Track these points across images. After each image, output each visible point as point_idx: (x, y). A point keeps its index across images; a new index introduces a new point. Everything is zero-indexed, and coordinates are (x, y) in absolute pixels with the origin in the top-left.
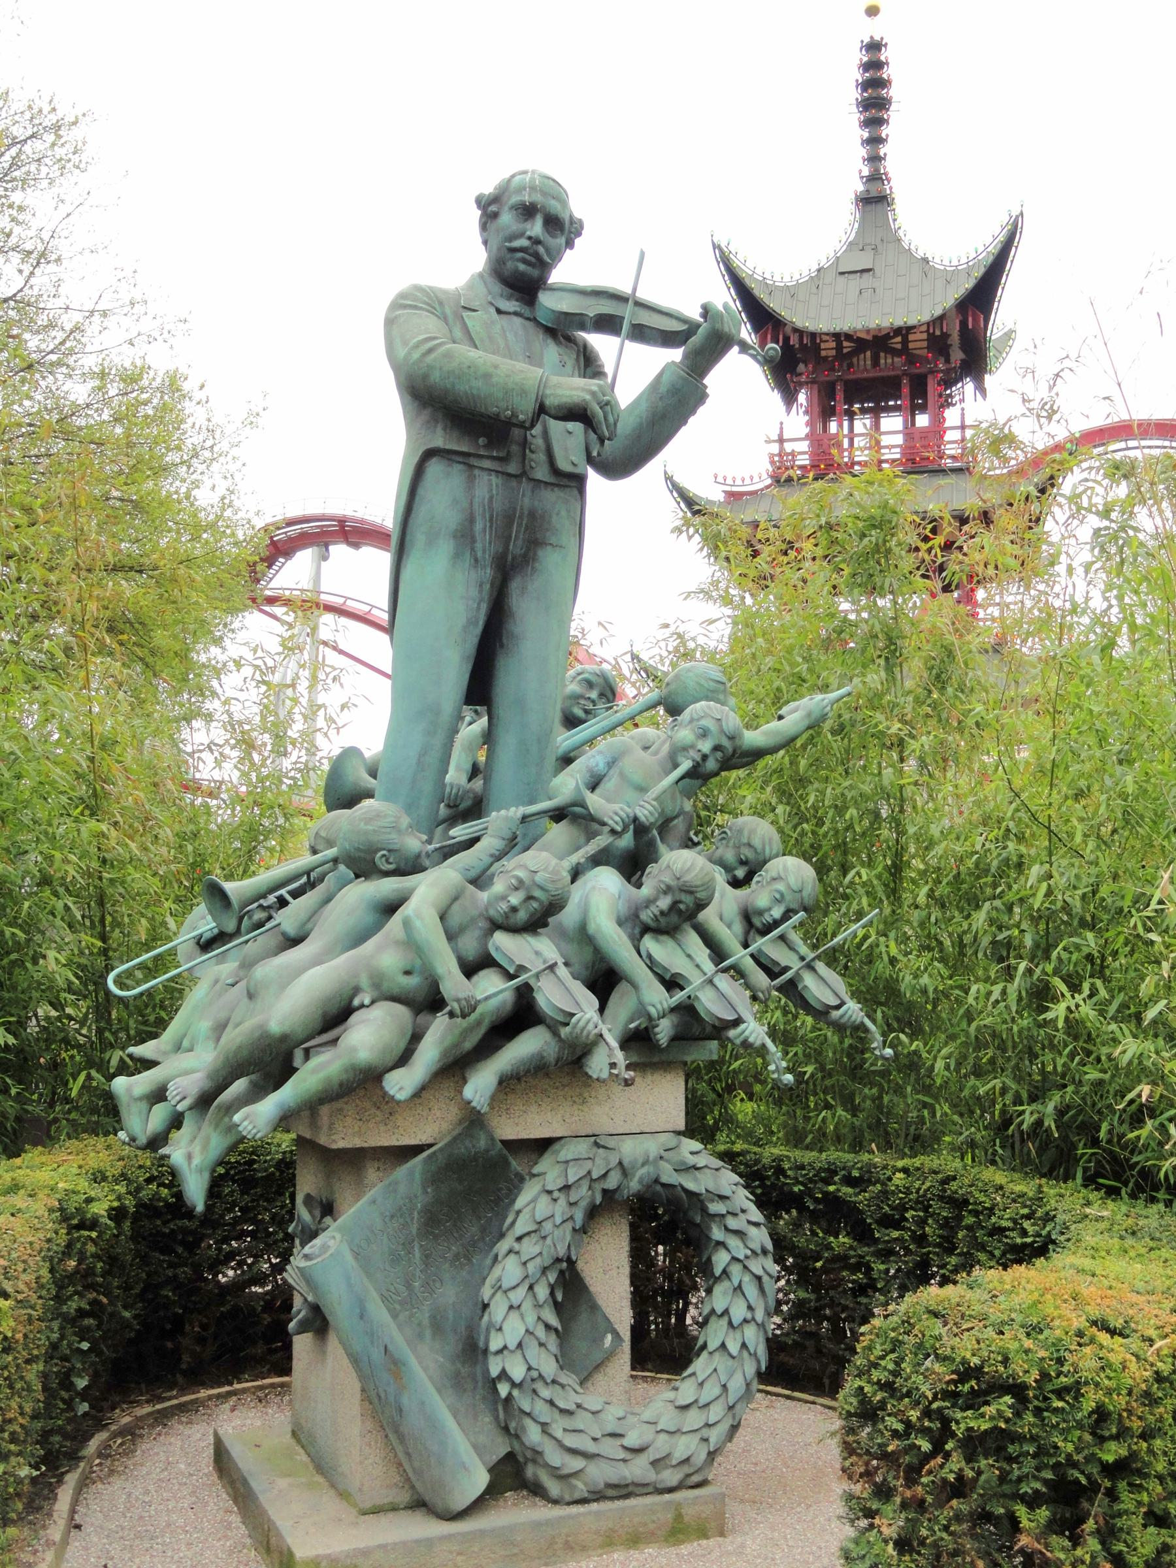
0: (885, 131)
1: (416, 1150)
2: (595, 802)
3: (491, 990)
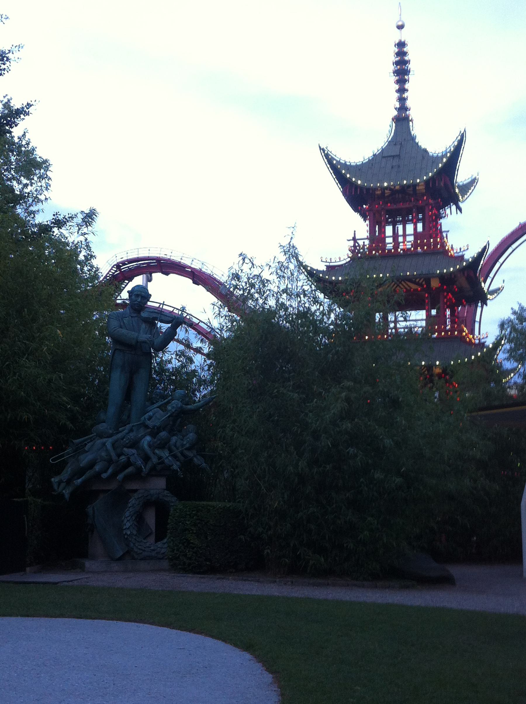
0: (407, 86)
1: (109, 490)
2: (148, 423)
3: (123, 458)
